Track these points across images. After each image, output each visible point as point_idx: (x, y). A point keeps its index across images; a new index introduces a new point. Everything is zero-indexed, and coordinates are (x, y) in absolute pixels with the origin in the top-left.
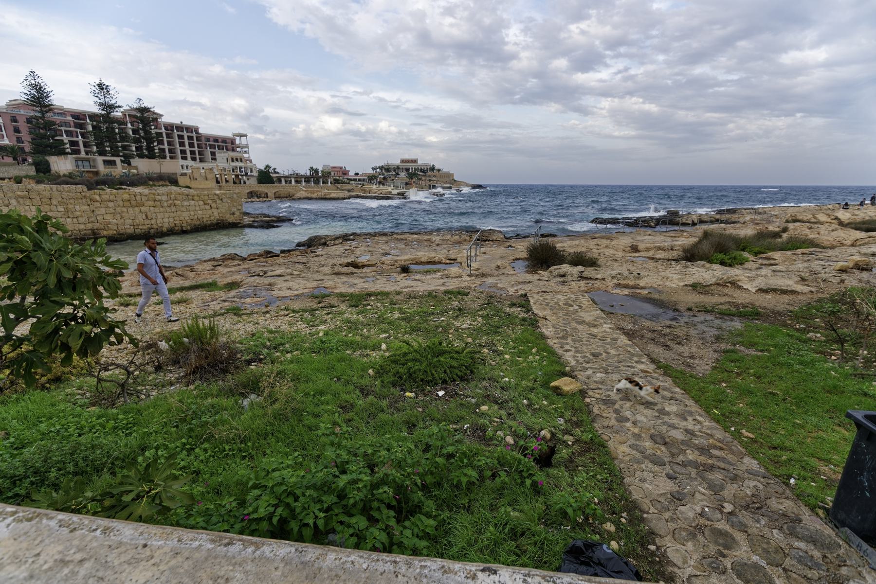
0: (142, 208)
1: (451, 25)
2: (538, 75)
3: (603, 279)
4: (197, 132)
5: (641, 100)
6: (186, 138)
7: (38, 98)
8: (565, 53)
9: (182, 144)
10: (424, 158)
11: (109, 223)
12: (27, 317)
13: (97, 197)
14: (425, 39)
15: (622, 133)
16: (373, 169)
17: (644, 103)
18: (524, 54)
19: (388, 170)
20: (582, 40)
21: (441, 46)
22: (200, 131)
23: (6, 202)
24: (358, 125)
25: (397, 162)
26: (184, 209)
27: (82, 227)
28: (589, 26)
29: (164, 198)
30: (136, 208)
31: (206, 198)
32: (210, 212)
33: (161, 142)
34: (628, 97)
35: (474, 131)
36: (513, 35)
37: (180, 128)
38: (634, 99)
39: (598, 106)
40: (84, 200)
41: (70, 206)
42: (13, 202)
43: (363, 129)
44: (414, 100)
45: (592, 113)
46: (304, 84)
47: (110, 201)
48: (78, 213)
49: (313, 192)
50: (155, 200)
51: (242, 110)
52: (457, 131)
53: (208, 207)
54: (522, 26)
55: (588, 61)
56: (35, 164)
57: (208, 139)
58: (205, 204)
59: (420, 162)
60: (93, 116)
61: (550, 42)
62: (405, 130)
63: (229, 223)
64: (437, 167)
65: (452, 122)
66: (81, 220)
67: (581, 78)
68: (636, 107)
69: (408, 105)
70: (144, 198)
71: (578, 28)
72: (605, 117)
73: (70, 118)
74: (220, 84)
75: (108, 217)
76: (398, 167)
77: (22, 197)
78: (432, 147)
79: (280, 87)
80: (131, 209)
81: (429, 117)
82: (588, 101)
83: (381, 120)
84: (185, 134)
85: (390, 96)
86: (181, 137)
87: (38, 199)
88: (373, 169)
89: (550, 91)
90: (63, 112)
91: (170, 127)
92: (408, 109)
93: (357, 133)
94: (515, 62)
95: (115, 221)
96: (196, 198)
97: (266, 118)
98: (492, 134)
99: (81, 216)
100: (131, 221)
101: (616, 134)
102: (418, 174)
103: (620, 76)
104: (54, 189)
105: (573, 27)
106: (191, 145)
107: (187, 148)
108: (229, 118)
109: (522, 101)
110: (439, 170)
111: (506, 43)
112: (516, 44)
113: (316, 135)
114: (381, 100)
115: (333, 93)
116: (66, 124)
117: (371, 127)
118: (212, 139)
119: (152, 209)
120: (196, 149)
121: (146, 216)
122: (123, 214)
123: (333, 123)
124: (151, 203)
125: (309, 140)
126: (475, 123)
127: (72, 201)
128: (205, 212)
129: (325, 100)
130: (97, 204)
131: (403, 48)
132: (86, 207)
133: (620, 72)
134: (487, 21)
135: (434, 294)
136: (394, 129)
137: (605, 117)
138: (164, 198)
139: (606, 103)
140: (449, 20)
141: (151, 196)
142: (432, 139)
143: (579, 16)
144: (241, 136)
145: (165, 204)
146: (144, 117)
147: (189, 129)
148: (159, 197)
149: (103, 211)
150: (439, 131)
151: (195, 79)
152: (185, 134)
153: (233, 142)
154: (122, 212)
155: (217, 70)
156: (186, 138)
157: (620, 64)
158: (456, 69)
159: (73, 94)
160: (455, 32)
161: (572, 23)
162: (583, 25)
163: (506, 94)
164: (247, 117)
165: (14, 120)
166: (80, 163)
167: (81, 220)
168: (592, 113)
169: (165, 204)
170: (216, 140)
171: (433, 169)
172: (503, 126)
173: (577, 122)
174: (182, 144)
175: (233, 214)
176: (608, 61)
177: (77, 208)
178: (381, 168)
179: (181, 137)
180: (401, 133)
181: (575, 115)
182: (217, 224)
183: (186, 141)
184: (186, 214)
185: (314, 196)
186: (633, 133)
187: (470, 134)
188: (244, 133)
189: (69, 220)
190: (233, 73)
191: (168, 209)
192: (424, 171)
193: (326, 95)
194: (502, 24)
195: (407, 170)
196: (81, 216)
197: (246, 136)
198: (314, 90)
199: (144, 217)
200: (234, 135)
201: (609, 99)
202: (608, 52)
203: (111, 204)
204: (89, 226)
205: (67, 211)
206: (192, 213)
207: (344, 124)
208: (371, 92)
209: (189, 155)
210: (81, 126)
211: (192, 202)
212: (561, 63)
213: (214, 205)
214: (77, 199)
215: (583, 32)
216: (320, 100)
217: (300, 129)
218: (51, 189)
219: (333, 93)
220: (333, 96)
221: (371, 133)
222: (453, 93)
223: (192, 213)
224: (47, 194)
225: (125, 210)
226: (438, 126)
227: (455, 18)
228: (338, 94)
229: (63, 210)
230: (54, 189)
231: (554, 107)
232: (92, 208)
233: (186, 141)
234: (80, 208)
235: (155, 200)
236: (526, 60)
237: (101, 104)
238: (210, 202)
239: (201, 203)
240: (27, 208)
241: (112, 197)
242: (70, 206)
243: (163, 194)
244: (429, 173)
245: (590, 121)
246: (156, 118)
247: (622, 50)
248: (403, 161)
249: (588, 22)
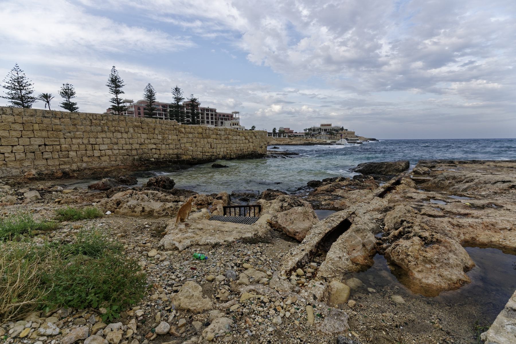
0: (209, 140)
1: (344, 51)
2: (403, 73)
4: (215, 112)
5: (485, 81)
6: (210, 115)
7: (150, 96)
8: (419, 59)
9: (208, 118)
10: (335, 124)
11: (188, 150)
13: (183, 130)
14: (329, 60)
15: (471, 104)
16: (304, 130)
17: (487, 83)
18: (392, 62)
19: (314, 130)
20: (435, 48)
21: (338, 63)
22: (217, 111)
23: (127, 130)
24: (290, 108)
25: (318, 125)
26: (233, 142)
27: (171, 152)
28: (439, 39)
29: (223, 133)
30: (205, 139)
31: (247, 135)
32: (248, 145)
33: (198, 117)
34: (474, 80)
35: (361, 108)
36: (385, 49)
37: (208, 110)
38: (479, 81)
39: (449, 87)
40: (175, 131)
41: (166, 136)
42: (131, 130)
43: (293, 110)
44: (322, 93)
45: (445, 93)
46: (262, 90)
47: (191, 133)
48: (170, 141)
49: (281, 141)
50: (217, 134)
51: (232, 104)
52: (349, 109)
53: (247, 141)
54: (390, 46)
55: (440, 59)
57: (220, 115)
58: (246, 139)
59: (333, 126)
60: (171, 106)
61: (410, 51)
62: (317, 110)
63: (259, 154)
64: (345, 128)
65: (347, 104)
66: (172, 146)
67: (435, 71)
68: (481, 86)
69: (319, 96)
70: (211, 132)
71: (431, 41)
72: (456, 94)
73: (161, 107)
74: (224, 93)
75: (188, 145)
76: (320, 129)
77: (137, 127)
78: (335, 118)
79: (250, 92)
80: (202, 140)
81: (332, 102)
82: (439, 86)
83: (303, 105)
84: (210, 113)
85: (307, 92)
86: (207, 114)
87: (147, 129)
88: (304, 130)
89: (408, 81)
90: (159, 104)
91: (203, 110)
92: (319, 98)
93: (290, 113)
94: (386, 67)
95: (191, 148)
96: (241, 134)
97: (243, 107)
98: (372, 110)
99: (172, 143)
100: (201, 149)
101: (466, 104)
102: (334, 133)
103: (467, 67)
104: (158, 122)
105: (427, 42)
106: (212, 118)
107: (210, 120)
108: (226, 108)
109: (392, 89)
110: (346, 130)
111: (380, 57)
112: (387, 56)
113: (267, 114)
114: (303, 94)
115: (277, 93)
116: (159, 110)
117: (297, 109)
119: (215, 140)
120: (214, 120)
121: (211, 145)
122: (197, 144)
123: (277, 108)
124: (214, 136)
125: (264, 118)
126: (360, 103)
127: (167, 132)
128: (245, 145)
129: (273, 97)
130: (182, 135)
131: (316, 66)
132: (175, 137)
133: (466, 64)
134: (367, 46)
136: (310, 110)
137: (456, 94)
138: (223, 133)
139: (455, 86)
140: (343, 48)
141: (215, 131)
142: (333, 114)
143: (431, 34)
144: (236, 113)
145: (223, 138)
147: (212, 110)
148: (220, 132)
149: (185, 140)
150: (338, 110)
151: (211, 91)
152: (210, 113)
153: (232, 116)
154: (197, 142)
155: (222, 86)
156: (210, 115)
157: (466, 59)
158: (348, 74)
159: (164, 98)
160: (348, 55)
161: (427, 39)
162: (435, 40)
163: (381, 86)
164: (235, 105)
165: (139, 109)
167: (172, 146)
168: (445, 93)
169: (223, 138)
170: (224, 116)
171: (342, 129)
172: (380, 104)
173: (433, 99)
174: (208, 118)
175: (262, 147)
176: (457, 59)
177: (170, 137)
178: (310, 130)
179: (207, 114)
180: (314, 112)
181: (433, 94)
182: (252, 154)
183: (210, 116)
184: (234, 146)
185: (282, 143)
186: (481, 104)
187: (358, 110)
188: (238, 111)
189: (164, 146)
190: (229, 87)
191: (224, 142)
192: (337, 131)
193: (274, 94)
194: (379, 47)
195: (325, 130)
196: (172, 143)
197: (238, 113)
198: (268, 92)
199: (209, 147)
200: (233, 113)
201: (458, 83)
202: (456, 53)
203: (191, 136)
204: (176, 151)
205: (164, 138)
206: (238, 145)
207: (282, 108)
208: (298, 91)
210: (165, 111)
211: (239, 137)
212: (420, 64)
213: (251, 140)
214: (171, 130)
215: (435, 43)
216: (271, 97)
217: (259, 113)
218: (156, 121)
219: (277, 93)
220: (278, 94)
221: (298, 112)
222: (346, 87)
223: (238, 145)
224: (153, 125)
225: (198, 140)
226: (338, 107)
227: (346, 46)
228: (280, 93)
229: (161, 138)
230: (158, 122)
231: (415, 91)
232: (179, 137)
233: (210, 116)
234: (172, 137)
235: (217, 134)
236: (394, 65)
237: (175, 98)
238: (249, 137)
239: (244, 138)
240: (139, 135)
241: (192, 130)
242: (166, 136)
243: (222, 130)
244: (340, 132)
245: (444, 99)
246: (198, 104)
247: (468, 51)
248: (322, 125)
249: (437, 37)
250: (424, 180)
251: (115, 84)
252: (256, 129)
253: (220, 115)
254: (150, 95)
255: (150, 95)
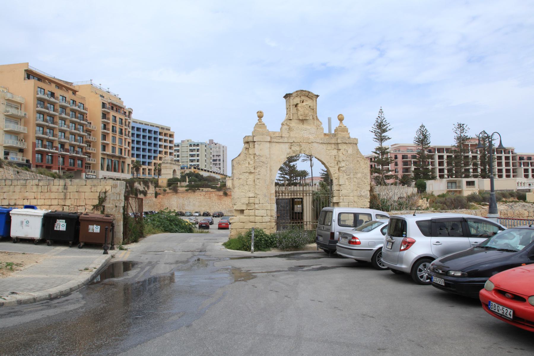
3: (223, 287)
6: (503, 158)
12: (126, 288)
22: (515, 151)
56: (417, 185)
86: (500, 158)
106: (507, 164)
107: (504, 167)
118: (525, 157)
120: (511, 167)
135: (72, 174)
146: (485, 143)
152: (503, 155)
156: (503, 158)
159: (443, 138)
166: (450, 185)
174: (500, 164)
179: (441, 157)
183: (504, 161)
209: (504, 173)
233: (504, 161)
250: (340, 255)
251: (381, 129)
252: (103, 251)
253: (521, 158)
254: (423, 139)
255: (423, 139)
